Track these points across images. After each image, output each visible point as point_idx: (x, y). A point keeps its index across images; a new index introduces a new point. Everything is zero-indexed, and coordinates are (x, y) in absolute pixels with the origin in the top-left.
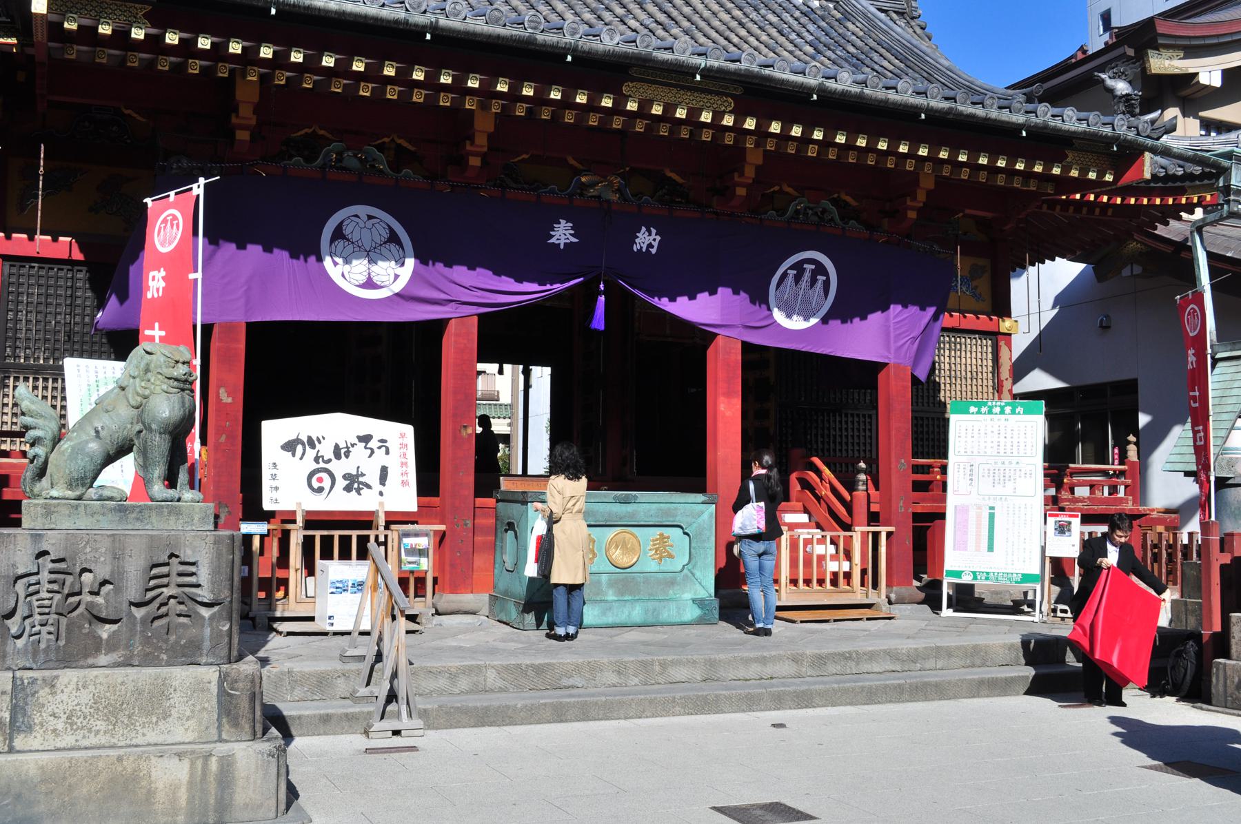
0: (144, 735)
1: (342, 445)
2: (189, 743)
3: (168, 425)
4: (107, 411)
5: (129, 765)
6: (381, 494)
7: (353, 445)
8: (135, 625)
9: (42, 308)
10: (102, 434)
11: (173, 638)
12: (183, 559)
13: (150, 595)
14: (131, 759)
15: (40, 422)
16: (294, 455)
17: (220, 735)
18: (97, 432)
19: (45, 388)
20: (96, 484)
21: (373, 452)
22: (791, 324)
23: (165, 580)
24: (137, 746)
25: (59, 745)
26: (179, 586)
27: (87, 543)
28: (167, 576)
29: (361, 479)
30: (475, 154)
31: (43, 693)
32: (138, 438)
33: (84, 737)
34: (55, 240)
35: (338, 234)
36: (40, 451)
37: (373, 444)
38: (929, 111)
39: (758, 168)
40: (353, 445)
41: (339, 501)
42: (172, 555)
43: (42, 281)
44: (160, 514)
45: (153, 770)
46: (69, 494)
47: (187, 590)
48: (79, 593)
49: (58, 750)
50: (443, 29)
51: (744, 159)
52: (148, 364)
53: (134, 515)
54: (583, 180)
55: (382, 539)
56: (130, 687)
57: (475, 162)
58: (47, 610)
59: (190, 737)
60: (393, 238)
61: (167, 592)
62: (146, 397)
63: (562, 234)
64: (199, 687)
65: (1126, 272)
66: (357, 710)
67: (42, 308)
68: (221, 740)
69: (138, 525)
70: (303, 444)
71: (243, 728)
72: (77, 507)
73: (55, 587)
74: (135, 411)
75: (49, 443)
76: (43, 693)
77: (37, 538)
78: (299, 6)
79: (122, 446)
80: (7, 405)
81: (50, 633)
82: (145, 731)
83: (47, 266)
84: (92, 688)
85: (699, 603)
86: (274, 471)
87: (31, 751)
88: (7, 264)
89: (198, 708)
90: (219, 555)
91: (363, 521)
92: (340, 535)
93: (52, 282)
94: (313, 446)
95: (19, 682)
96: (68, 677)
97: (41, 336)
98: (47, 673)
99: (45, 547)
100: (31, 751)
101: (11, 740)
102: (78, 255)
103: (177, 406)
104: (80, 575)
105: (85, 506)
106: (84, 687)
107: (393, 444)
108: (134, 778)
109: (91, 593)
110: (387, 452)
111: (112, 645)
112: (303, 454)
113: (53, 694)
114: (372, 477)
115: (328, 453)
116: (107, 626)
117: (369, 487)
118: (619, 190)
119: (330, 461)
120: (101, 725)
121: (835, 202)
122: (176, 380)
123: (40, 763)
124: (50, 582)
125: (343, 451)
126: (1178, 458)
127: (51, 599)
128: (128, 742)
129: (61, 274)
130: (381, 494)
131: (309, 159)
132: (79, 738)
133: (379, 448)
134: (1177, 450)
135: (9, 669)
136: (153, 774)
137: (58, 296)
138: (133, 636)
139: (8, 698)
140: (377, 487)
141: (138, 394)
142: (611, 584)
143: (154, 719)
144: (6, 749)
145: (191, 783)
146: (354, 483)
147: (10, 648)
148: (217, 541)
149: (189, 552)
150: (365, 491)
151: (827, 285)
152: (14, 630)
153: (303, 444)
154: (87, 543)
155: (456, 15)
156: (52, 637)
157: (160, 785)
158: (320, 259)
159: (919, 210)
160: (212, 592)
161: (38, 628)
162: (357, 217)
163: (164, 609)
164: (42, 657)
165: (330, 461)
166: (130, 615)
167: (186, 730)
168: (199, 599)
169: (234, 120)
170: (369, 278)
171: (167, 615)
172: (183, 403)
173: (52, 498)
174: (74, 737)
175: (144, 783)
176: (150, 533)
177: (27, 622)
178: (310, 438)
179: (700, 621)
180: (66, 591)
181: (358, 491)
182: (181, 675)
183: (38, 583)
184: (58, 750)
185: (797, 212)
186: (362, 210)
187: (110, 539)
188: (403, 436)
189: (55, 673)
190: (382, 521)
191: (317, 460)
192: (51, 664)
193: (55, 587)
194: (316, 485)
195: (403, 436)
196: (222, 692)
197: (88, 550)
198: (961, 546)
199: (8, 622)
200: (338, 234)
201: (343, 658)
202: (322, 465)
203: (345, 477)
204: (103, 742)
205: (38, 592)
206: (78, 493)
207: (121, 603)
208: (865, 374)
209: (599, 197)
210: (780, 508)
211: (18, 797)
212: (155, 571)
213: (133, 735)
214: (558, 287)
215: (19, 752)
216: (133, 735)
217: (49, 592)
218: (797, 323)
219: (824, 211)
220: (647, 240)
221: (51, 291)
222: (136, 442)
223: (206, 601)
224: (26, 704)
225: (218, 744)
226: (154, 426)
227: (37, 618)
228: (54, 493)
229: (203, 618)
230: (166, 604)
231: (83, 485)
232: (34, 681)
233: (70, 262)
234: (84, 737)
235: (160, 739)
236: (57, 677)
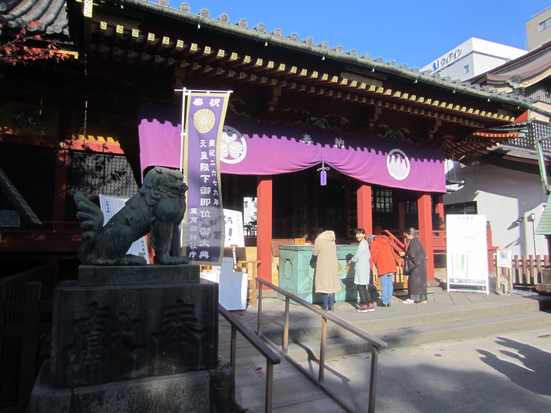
6: (230, 240)
10: (131, 222)
30: (272, 106)
38: (457, 90)
39: (379, 115)
50: (273, 42)
51: (374, 112)
54: (312, 119)
57: (272, 109)
62: (157, 200)
65: (473, 164)
74: (151, 209)
78: (211, 26)
89: (197, 402)
105: (121, 269)
110: (232, 223)
113: (101, 404)
118: (325, 124)
121: (402, 131)
126: (542, 230)
130: (230, 240)
134: (540, 226)
141: (153, 198)
155: (279, 36)
159: (434, 135)
173: (99, 265)
188: (238, 216)
195: (238, 216)
197: (124, 300)
206: (115, 261)
209: (318, 126)
219: (399, 134)
222: (152, 228)
223: (199, 329)
226: (163, 218)
228: (100, 261)
232: (86, 397)
236: (103, 392)
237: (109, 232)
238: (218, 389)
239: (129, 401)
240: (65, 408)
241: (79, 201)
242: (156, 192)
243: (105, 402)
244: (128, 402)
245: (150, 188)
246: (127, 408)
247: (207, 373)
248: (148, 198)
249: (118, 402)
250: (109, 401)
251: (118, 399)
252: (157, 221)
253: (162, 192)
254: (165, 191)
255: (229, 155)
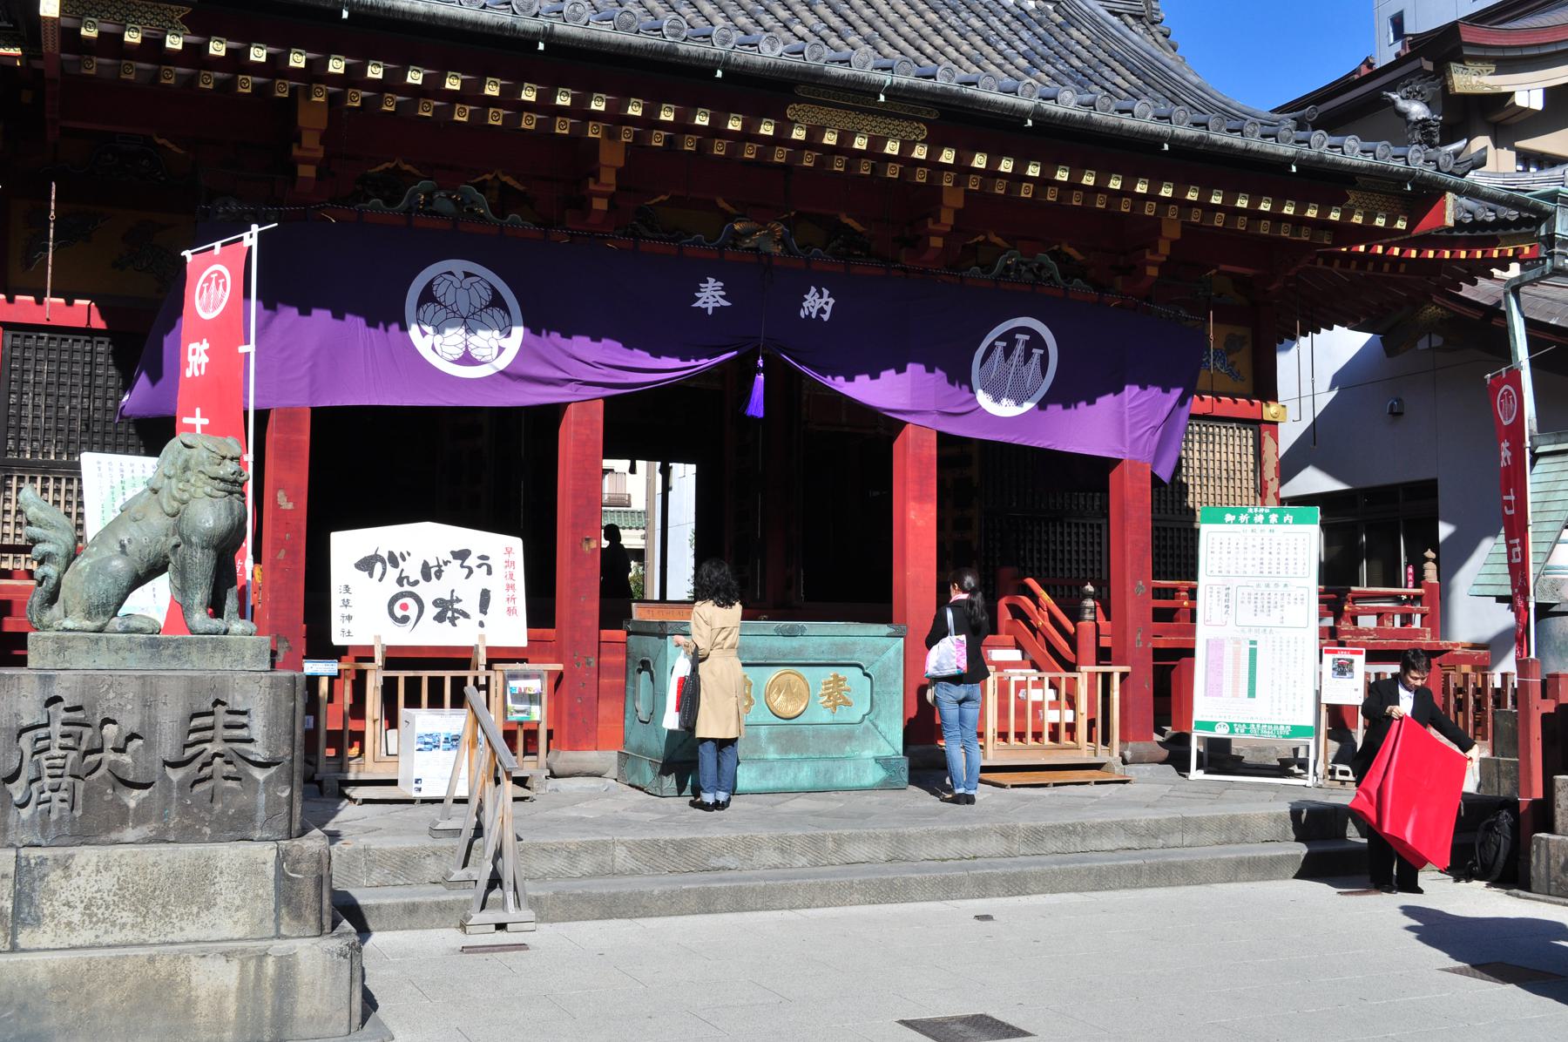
0: (182, 929)
1: (432, 563)
2: (239, 940)
3: (212, 537)
4: (136, 520)
5: (163, 967)
6: (481, 624)
7: (446, 563)
8: (170, 791)
9: (53, 389)
10: (129, 548)
11: (218, 807)
12: (231, 707)
13: (190, 752)
14: (166, 959)
15: (51, 533)
16: (371, 575)
17: (278, 930)
18: (123, 546)
19: (57, 491)
20: (121, 612)
21: (471, 571)
22: (1000, 410)
23: (209, 734)
24: (173, 943)
25: (74, 942)
26: (227, 741)
27: (111, 686)
28: (211, 728)
29: (456, 606)
30: (601, 195)
31: (55, 876)
32: (174, 554)
33: (106, 932)
34: (69, 303)
35: (427, 296)
36: (51, 570)
37: (472, 561)
38: (1174, 140)
39: (957, 212)
40: (446, 563)
41: (429, 634)
42: (217, 702)
43: (53, 356)
44: (202, 650)
45: (194, 974)
46: (87, 624)
47: (236, 746)
48: (100, 750)
49: (74, 948)
50: (560, 37)
51: (940, 202)
52: (187, 461)
53: (169, 652)
54: (737, 227)
55: (482, 681)
56: (165, 868)
57: (600, 204)
58: (59, 772)
59: (239, 932)
60: (497, 301)
61: (211, 748)
62: (184, 502)
63: (711, 296)
64: (252, 869)
65: (1423, 344)
66: (451, 898)
67: (53, 389)
68: (279, 936)
69: (174, 664)
70: (383, 562)
71: (307, 921)
72: (97, 641)
73: (70, 742)
74: (171, 520)
75: (62, 560)
76: (55, 876)
77: (46, 680)
78: (378, 8)
79: (154, 565)
80: (9, 512)
81: (63, 801)
82: (183, 924)
83: (59, 336)
84: (116, 870)
85: (883, 762)
86: (347, 596)
87: (39, 950)
88: (9, 334)
89: (250, 895)
90: (277, 702)
91: (459, 659)
92: (430, 676)
93: (65, 357)
94: (395, 564)
95: (24, 863)
96: (86, 856)
97: (52, 425)
98: (59, 851)
99: (57, 692)
100: (39, 950)
101: (14, 936)
102: (98, 323)
103: (224, 514)
104: (101, 728)
105: (108, 640)
106: (106, 869)
107: (496, 562)
108: (170, 984)
109: (116, 750)
110: (489, 572)
111: (141, 816)
112: (383, 574)
113: (67, 877)
114: (470, 604)
115: (414, 573)
116: (136, 792)
117: (466, 615)
118: (782, 241)
119: (416, 582)
120: (127, 917)
121: (1055, 255)
122: (223, 480)
123: (51, 965)
124: (63, 736)
125: (433, 571)
126: (1488, 580)
127: (64, 757)
128: (162, 938)
129: (77, 346)
130: (481, 624)
131: (391, 201)
132: (100, 933)
133: (479, 566)
134: (1488, 569)
135: (11, 846)
136: (194, 979)
137: (73, 374)
138: (167, 804)
139: (9, 883)
140: (476, 615)
141: (175, 499)
142: (772, 739)
143: (195, 909)
144: (8, 947)
145: (241, 990)
146: (447, 610)
147: (12, 820)
148: (274, 685)
149: (239, 698)
150: (461, 621)
151: (1044, 360)
152: (18, 797)
153: (383, 562)
154: (111, 686)
155: (577, 19)
156: (66, 805)
157: (202, 993)
158: (404, 328)
159: (1161, 266)
160: (268, 748)
161: (47, 794)
162: (451, 274)
163: (207, 771)
164: (53, 831)
165: (416, 582)
166: (165, 778)
167: (236, 923)
168: (252, 758)
169: (296, 152)
170: (466, 352)
171: (211, 777)
172: (232, 509)
173: (66, 630)
174: (93, 933)
175: (182, 990)
176: (189, 673)
177: (35, 786)
178: (391, 554)
179: (885, 786)
180: (83, 748)
181: (453, 621)
182: (228, 854)
183: (48, 737)
184: (74, 948)
185: (1007, 268)
186: (458, 266)
187: (139, 682)
188: (509, 551)
189: (70, 850)
190: (482, 659)
191: (400, 581)
192: (65, 840)
193: (70, 742)
194: (399, 613)
195: (509, 551)
196: (281, 875)
197: (111, 695)
198: (1214, 690)
199: (11, 787)
200: (427, 296)
201: (434, 832)
202: (407, 588)
203: (435, 603)
204: (130, 938)
205: (48, 749)
206: (99, 623)
207: (153, 763)
208: (1093, 474)
209: (757, 249)
210: (985, 642)
211: (23, 1008)
212: (196, 722)
213: (168, 929)
214: (705, 363)
215: (23, 950)
216: (168, 929)
217: (61, 748)
218: (1007, 409)
219: (1041, 267)
220: (817, 303)
221: (64, 368)
222: (172, 559)
223: (260, 759)
224: (33, 890)
225: (276, 941)
226: (194, 539)
227: (47, 781)
228: (69, 624)
229: (257, 781)
230: (210, 764)
231: (105, 613)
232: (42, 861)
233: (89, 332)
234: (106, 932)
235: (202, 935)
236: (72, 856)
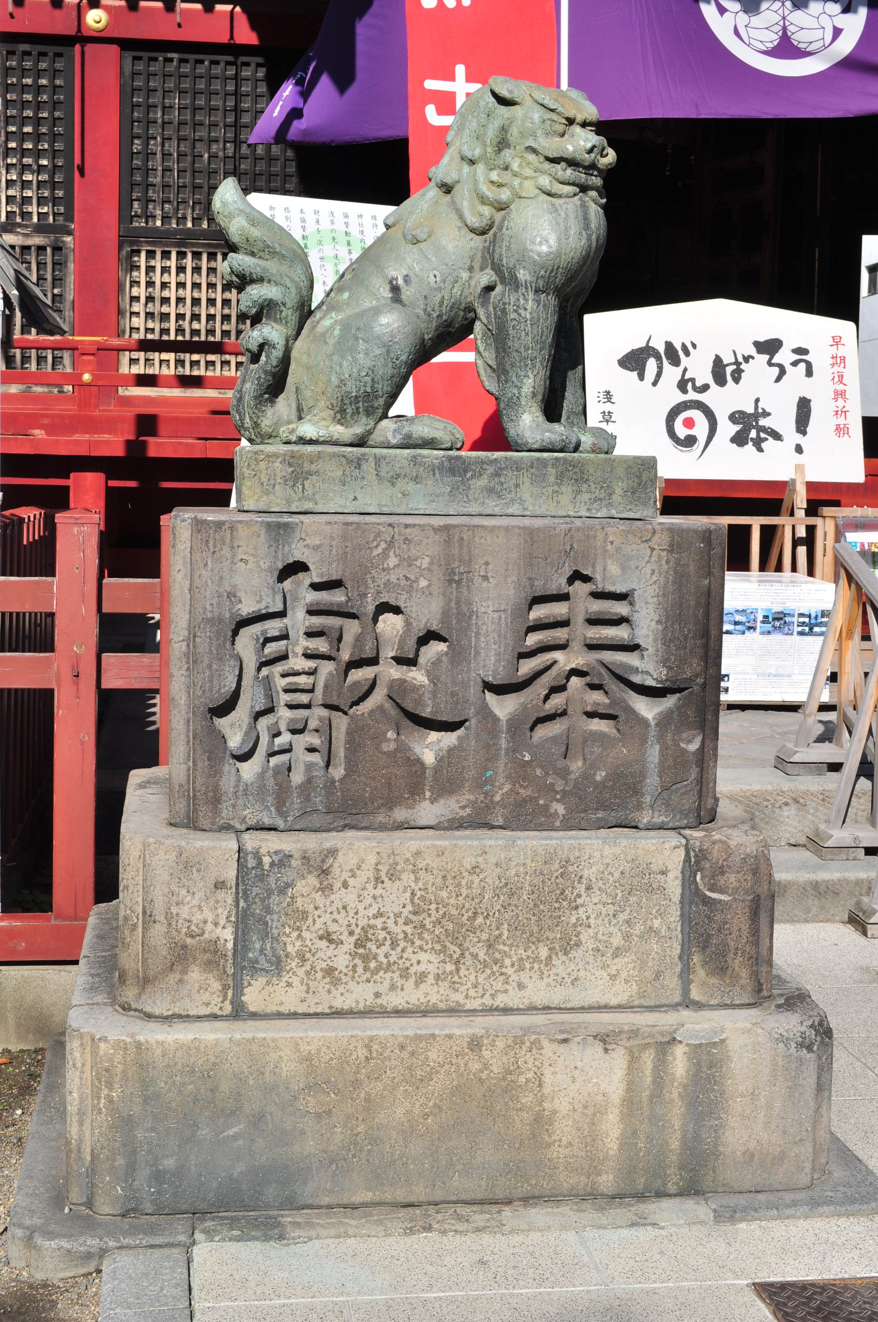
0: (521, 986)
1: (728, 358)
2: (620, 1008)
3: (554, 270)
4: (416, 241)
5: (495, 1058)
6: (799, 449)
7: (747, 359)
8: (494, 733)
9: (186, 131)
10: (407, 293)
11: (576, 766)
12: (602, 585)
13: (527, 667)
14: (500, 1044)
15: (271, 266)
16: (641, 377)
17: (686, 992)
18: (395, 289)
19: (197, 270)
20: (392, 413)
21: (782, 372)
23: (560, 634)
24: (506, 1011)
25: (339, 1003)
26: (592, 647)
27: (391, 544)
28: (564, 623)
29: (763, 422)
31: (305, 887)
32: (485, 303)
33: (393, 987)
34: (209, 8)
36: (272, 332)
37: (784, 356)
40: (747, 359)
41: (725, 462)
42: (577, 576)
43: (186, 85)
44: (539, 479)
45: (547, 1071)
46: (339, 431)
47: (608, 656)
48: (373, 661)
49: (338, 1014)
52: (504, 129)
53: (483, 482)
55: (802, 533)
56: (491, 877)
58: (304, 698)
59: (619, 994)
61: (564, 660)
62: (502, 207)
64: (641, 882)
66: (836, 876)
67: (186, 131)
68: (688, 1003)
69: (492, 505)
70: (658, 357)
71: (735, 977)
72: (358, 463)
73: (321, 645)
75: (290, 314)
76: (305, 887)
77: (279, 531)
79: (449, 324)
80: (137, 299)
81: (311, 750)
82: (524, 977)
83: (192, 57)
84: (408, 878)
86: (608, 407)
87: (279, 1015)
88: (129, 56)
89: (638, 929)
90: (680, 577)
91: (767, 500)
93: (201, 85)
94: (675, 361)
95: (251, 863)
96: (357, 850)
97: (187, 180)
98: (311, 842)
99: (298, 554)
100: (279, 1015)
101: (239, 990)
102: (246, 35)
103: (574, 228)
104: (375, 620)
105: (378, 460)
106: (392, 876)
107: (819, 358)
108: (507, 1086)
109: (399, 660)
110: (809, 373)
111: (446, 779)
112: (659, 375)
113: (326, 889)
114: (782, 419)
115: (702, 374)
116: (434, 736)
117: (777, 436)
119: (705, 388)
120: (428, 962)
122: (572, 163)
123: (304, 1047)
124: (310, 635)
125: (729, 370)
127: (312, 673)
128: (488, 1001)
129: (217, 70)
130: (799, 449)
132: (384, 988)
133: (795, 364)
135: (227, 828)
136: (548, 1079)
137: (212, 109)
138: (491, 759)
139: (227, 896)
143: (544, 952)
144: (228, 1008)
145: (630, 1102)
146: (750, 428)
147: (227, 783)
148: (677, 542)
149: (614, 569)
150: (770, 444)
152: (235, 741)
153: (658, 357)
154: (391, 544)
156: (316, 758)
157: (562, 1105)
160: (665, 662)
161: (285, 738)
163: (557, 701)
164: (295, 802)
165: (705, 388)
166: (486, 714)
167: (613, 977)
168: (637, 679)
171: (564, 713)
172: (586, 218)
173: (303, 441)
174: (371, 988)
175: (527, 1099)
176: (527, 522)
177: (264, 723)
178: (669, 346)
180: (345, 655)
181: (758, 444)
182: (600, 852)
183: (285, 637)
184: (338, 1014)
187: (439, 538)
188: (837, 341)
189: (331, 840)
190: (801, 500)
191: (682, 386)
192: (316, 820)
193: (321, 645)
194: (681, 432)
196: (692, 896)
197: (392, 561)
199: (222, 723)
201: (782, 764)
202: (692, 395)
203: (734, 418)
204: (434, 999)
205: (284, 657)
206: (358, 430)
207: (465, 685)
211: (258, 1120)
212: (539, 612)
213: (498, 985)
215: (254, 1016)
216: (498, 985)
217: (308, 656)
221: (201, 102)
222: (481, 312)
223: (650, 682)
224: (268, 910)
225: (685, 1013)
226: (523, 275)
227: (284, 714)
228: (308, 430)
229: (644, 722)
230: (561, 688)
231: (369, 413)
232: (283, 860)
233: (233, 51)
234: (393, 987)
235: (556, 997)
236: (333, 852)
237: (332, 328)
238: (714, 895)
239: (413, 894)
240: (220, 885)
241: (230, 216)
242: (494, 176)
243: (338, 885)
244: (408, 894)
245: (472, 162)
246: (405, 912)
247: (673, 839)
248: (464, 197)
249: (379, 891)
250: (351, 882)
251: (378, 880)
252: (499, 289)
253: (515, 175)
254: (528, 172)
255: (785, 38)
